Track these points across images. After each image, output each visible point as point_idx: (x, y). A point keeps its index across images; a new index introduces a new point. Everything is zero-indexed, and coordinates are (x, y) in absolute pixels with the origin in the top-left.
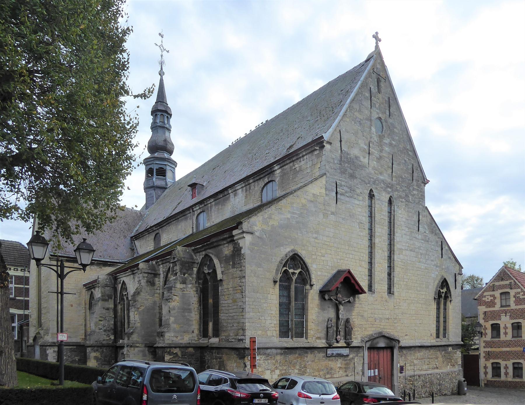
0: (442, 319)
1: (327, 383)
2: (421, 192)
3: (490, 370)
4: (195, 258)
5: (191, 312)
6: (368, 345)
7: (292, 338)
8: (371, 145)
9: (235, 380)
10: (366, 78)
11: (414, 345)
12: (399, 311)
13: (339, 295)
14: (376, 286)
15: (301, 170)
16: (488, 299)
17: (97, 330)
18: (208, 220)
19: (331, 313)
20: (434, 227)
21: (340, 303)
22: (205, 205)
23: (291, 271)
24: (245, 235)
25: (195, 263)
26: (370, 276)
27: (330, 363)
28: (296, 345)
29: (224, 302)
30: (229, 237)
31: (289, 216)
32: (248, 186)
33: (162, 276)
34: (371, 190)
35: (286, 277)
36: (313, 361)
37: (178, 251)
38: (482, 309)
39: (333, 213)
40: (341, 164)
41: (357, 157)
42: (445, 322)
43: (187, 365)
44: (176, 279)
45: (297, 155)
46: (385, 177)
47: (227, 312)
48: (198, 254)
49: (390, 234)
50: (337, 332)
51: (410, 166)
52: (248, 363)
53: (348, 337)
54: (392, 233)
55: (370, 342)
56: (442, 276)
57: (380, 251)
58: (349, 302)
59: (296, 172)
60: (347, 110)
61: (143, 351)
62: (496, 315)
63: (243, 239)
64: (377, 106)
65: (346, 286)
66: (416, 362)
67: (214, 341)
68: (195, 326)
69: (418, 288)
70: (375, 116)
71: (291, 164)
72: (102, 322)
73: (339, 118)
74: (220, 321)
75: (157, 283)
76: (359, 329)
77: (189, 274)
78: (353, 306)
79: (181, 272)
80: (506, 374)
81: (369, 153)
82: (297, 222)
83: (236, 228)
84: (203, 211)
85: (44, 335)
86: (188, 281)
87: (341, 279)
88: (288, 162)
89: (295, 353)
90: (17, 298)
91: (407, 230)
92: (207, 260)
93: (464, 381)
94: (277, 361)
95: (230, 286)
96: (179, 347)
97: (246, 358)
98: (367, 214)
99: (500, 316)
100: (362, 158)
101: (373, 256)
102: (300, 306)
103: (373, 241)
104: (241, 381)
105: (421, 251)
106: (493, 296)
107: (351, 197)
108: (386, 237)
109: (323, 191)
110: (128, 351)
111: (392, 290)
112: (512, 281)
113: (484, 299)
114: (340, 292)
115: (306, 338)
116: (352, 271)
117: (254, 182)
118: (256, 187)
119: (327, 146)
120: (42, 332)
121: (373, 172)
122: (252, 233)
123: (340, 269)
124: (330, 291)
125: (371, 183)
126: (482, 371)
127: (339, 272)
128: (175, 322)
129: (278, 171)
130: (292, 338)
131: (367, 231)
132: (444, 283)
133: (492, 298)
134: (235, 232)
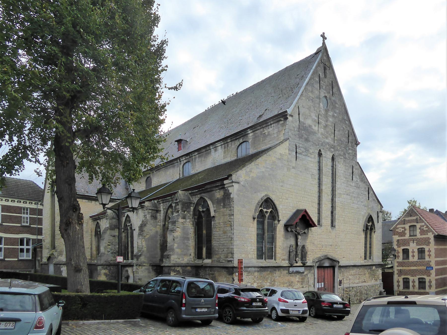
0: (368, 246)
1: (295, 291)
2: (354, 151)
3: (401, 284)
4: (192, 199)
5: (189, 240)
6: (317, 265)
7: (265, 259)
8: (320, 117)
9: (239, 289)
10: (316, 67)
11: (349, 265)
12: (339, 239)
13: (298, 228)
14: (323, 221)
15: (269, 135)
16: (400, 230)
17: (106, 253)
18: (193, 168)
19: (292, 241)
20: (363, 177)
21: (299, 234)
22: (190, 157)
23: (265, 210)
24: (233, 184)
25: (191, 203)
26: (319, 213)
27: (291, 278)
28: (268, 265)
29: (216, 233)
30: (221, 185)
31: (263, 170)
32: (226, 145)
33: (162, 212)
34: (320, 150)
35: (262, 214)
36: (280, 277)
37: (180, 194)
38: (396, 238)
39: (293, 168)
40: (299, 131)
41: (310, 126)
42: (370, 247)
43: (208, 279)
44: (178, 215)
45: (266, 123)
46: (329, 140)
47: (218, 240)
48: (194, 197)
49: (333, 183)
50: (296, 255)
51: (347, 132)
52: (236, 278)
53: (304, 259)
54: (334, 182)
55: (319, 263)
56: (369, 214)
57: (326, 195)
58: (305, 233)
59: (265, 136)
60: (303, 91)
61: (148, 269)
62: (406, 242)
63: (232, 187)
64: (324, 87)
65: (304, 221)
66: (350, 277)
67: (208, 261)
68: (192, 250)
69: (352, 223)
70: (322, 95)
71: (262, 130)
72: (110, 247)
73: (298, 97)
74: (213, 247)
75: (159, 217)
76: (311, 253)
77: (188, 212)
78: (307, 236)
79: (182, 210)
80: (414, 286)
81: (318, 123)
82: (269, 175)
83: (227, 179)
84: (188, 162)
85: (58, 256)
86: (187, 217)
87: (300, 216)
88: (259, 128)
89: (268, 271)
90: (32, 226)
91: (344, 179)
92: (203, 201)
93: (384, 291)
94: (255, 276)
95: (221, 221)
96: (181, 266)
97: (234, 274)
98: (317, 168)
99: (409, 243)
100: (313, 126)
101: (321, 198)
102: (271, 236)
103: (321, 188)
104: (244, 290)
105: (354, 195)
106: (404, 228)
107: (306, 155)
108: (330, 185)
109: (287, 151)
110: (137, 269)
111: (334, 224)
112: (418, 217)
113: (397, 230)
114: (298, 226)
115: (275, 260)
116: (308, 211)
117: (231, 141)
118: (233, 145)
119: (290, 118)
120: (56, 254)
121: (321, 137)
122: (239, 183)
123: (298, 209)
124: (292, 225)
125: (320, 144)
126: (395, 284)
127: (298, 211)
128: (178, 247)
129: (251, 135)
130: (265, 259)
131: (317, 181)
132: (370, 219)
133: (403, 230)
134: (225, 182)
